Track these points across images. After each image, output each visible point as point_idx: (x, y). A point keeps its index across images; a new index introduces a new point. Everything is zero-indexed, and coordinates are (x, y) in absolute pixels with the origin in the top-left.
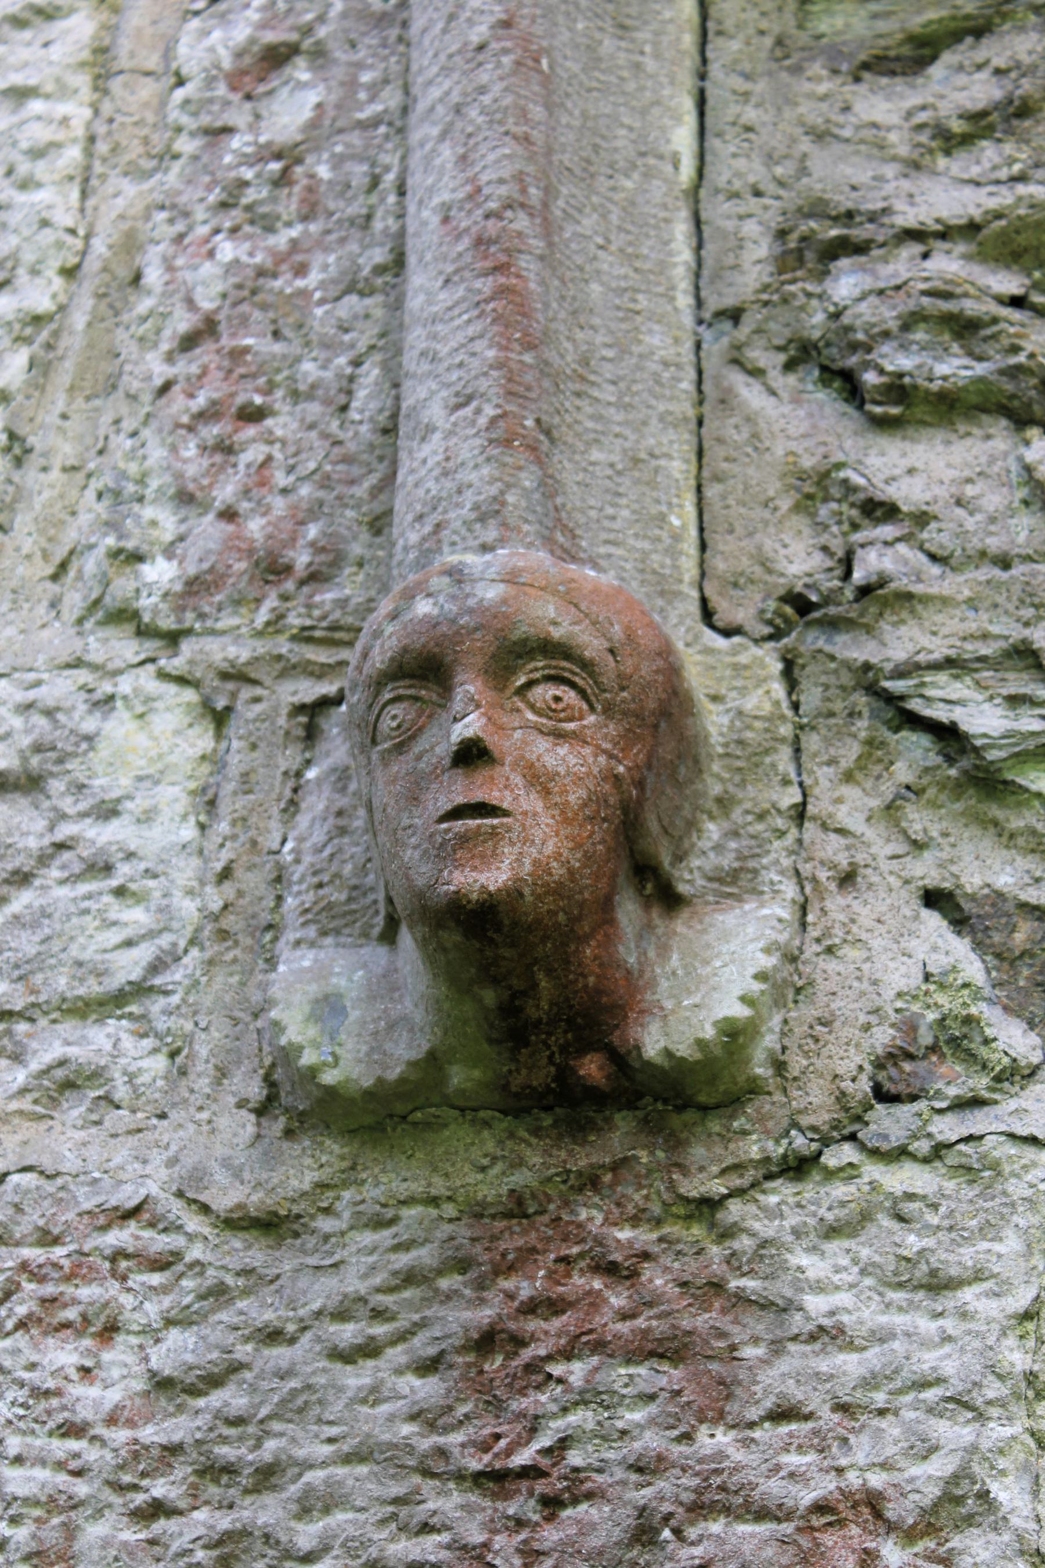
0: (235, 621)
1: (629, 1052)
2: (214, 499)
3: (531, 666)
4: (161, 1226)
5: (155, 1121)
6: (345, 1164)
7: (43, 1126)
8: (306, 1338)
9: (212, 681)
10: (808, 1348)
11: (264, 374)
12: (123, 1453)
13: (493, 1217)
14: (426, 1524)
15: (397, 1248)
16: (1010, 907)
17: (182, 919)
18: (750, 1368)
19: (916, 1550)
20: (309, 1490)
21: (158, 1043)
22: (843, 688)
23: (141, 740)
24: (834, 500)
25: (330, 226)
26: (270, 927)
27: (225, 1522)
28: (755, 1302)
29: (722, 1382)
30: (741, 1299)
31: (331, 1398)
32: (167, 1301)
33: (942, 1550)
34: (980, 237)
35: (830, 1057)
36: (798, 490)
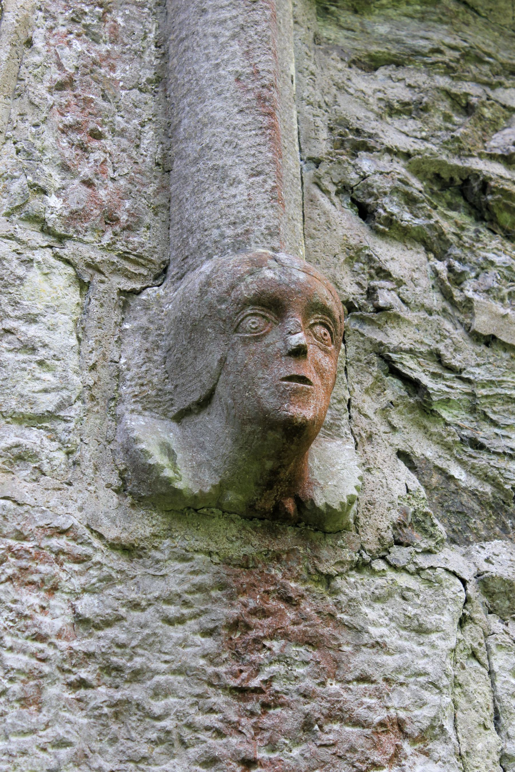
1: (307, 501)
2: (79, 173)
3: (316, 316)
4: (80, 541)
5: (66, 486)
6: (166, 527)
7: (10, 476)
8: (151, 609)
9: (81, 266)
10: (370, 650)
11: (101, 116)
12: (66, 653)
13: (235, 566)
14: (212, 709)
15: (195, 573)
16: (431, 466)
17: (74, 385)
18: (347, 656)
19: (416, 747)
20: (158, 685)
21: (61, 446)
23: (45, 286)
25: (124, 50)
26: (114, 399)
27: (118, 695)
28: (347, 626)
29: (335, 661)
30: (341, 624)
31: (165, 641)
32: (83, 580)
33: (425, 749)
34: (410, 160)
36: (347, 253)
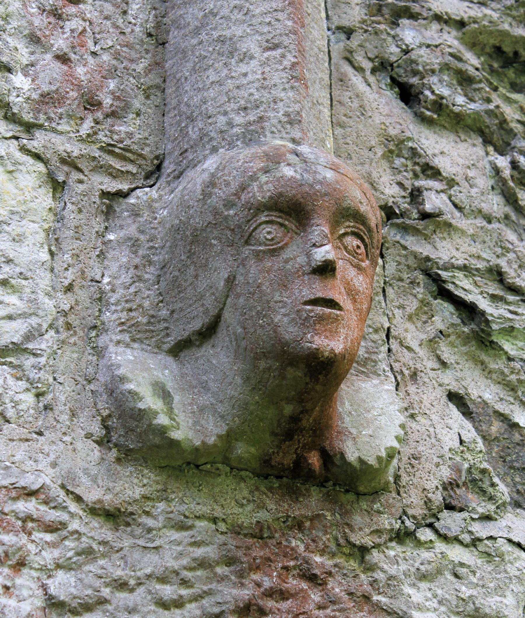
0: (67, 128)
1: (336, 455)
2: (52, 45)
4: (52, 505)
5: (35, 436)
6: (159, 487)
8: (141, 590)
9: (55, 161)
13: (245, 535)
15: (196, 544)
22: (408, 267)
24: (403, 157)
26: (95, 327)
32: (56, 553)
34: (464, 30)
35: (421, 478)
36: (385, 146)
